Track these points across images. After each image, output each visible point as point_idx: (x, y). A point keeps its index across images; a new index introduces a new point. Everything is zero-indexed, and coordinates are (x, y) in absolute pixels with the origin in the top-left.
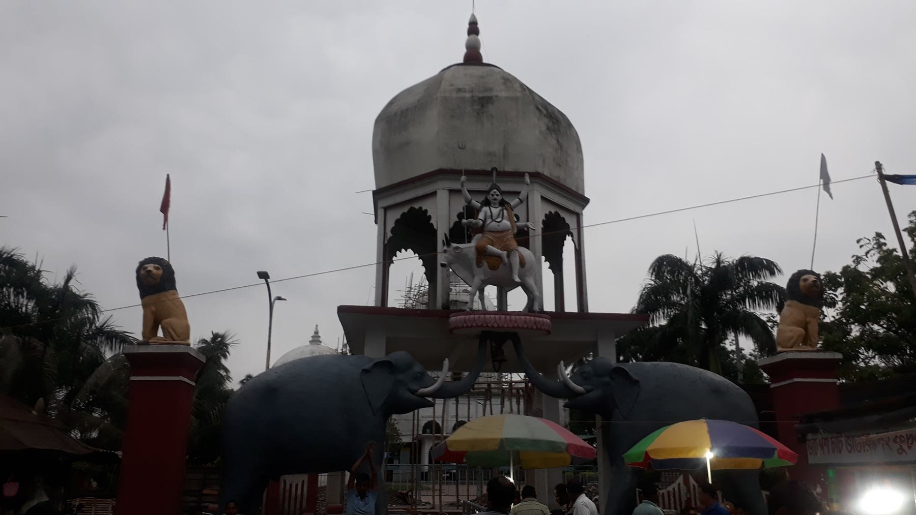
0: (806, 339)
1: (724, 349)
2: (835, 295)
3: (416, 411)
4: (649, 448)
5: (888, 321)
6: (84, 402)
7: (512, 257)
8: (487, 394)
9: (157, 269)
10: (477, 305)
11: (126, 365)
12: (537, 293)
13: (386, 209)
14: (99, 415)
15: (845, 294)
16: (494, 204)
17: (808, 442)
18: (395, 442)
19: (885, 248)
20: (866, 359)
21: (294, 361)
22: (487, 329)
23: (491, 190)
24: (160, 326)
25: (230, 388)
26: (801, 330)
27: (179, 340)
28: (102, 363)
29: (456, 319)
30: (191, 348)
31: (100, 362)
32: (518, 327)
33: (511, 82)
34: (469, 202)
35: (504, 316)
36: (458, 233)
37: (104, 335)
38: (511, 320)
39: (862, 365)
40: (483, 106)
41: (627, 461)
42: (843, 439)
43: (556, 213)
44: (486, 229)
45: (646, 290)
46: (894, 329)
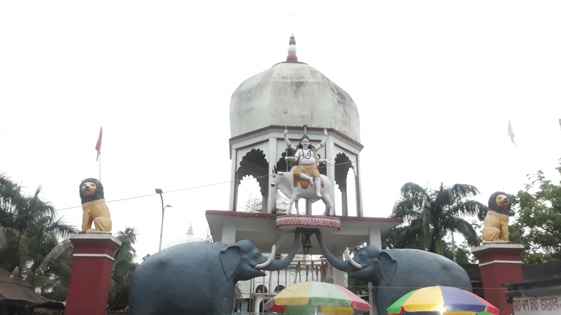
0: (501, 236)
1: (443, 242)
2: (514, 209)
3: (253, 279)
4: (404, 305)
5: (547, 225)
6: (44, 270)
7: (316, 181)
8: (298, 268)
9: (93, 185)
10: (294, 212)
11: (71, 247)
12: (331, 204)
13: (237, 150)
14: (53, 278)
15: (520, 208)
16: (305, 147)
17: (514, 303)
18: (238, 298)
19: (544, 180)
20: (534, 249)
21: (177, 245)
22: (300, 226)
23: (303, 139)
24: (93, 222)
25: (136, 262)
26: (498, 230)
27: (105, 231)
28: (56, 245)
29: (280, 219)
30: (112, 236)
31: (55, 244)
32: (320, 225)
33: (316, 73)
34: (289, 146)
35: (311, 218)
36: (282, 166)
37: (58, 227)
38: (315, 221)
39: (532, 252)
40: (298, 87)
41: (390, 312)
42: (539, 301)
44: (300, 163)
45: (397, 204)
46: (550, 230)
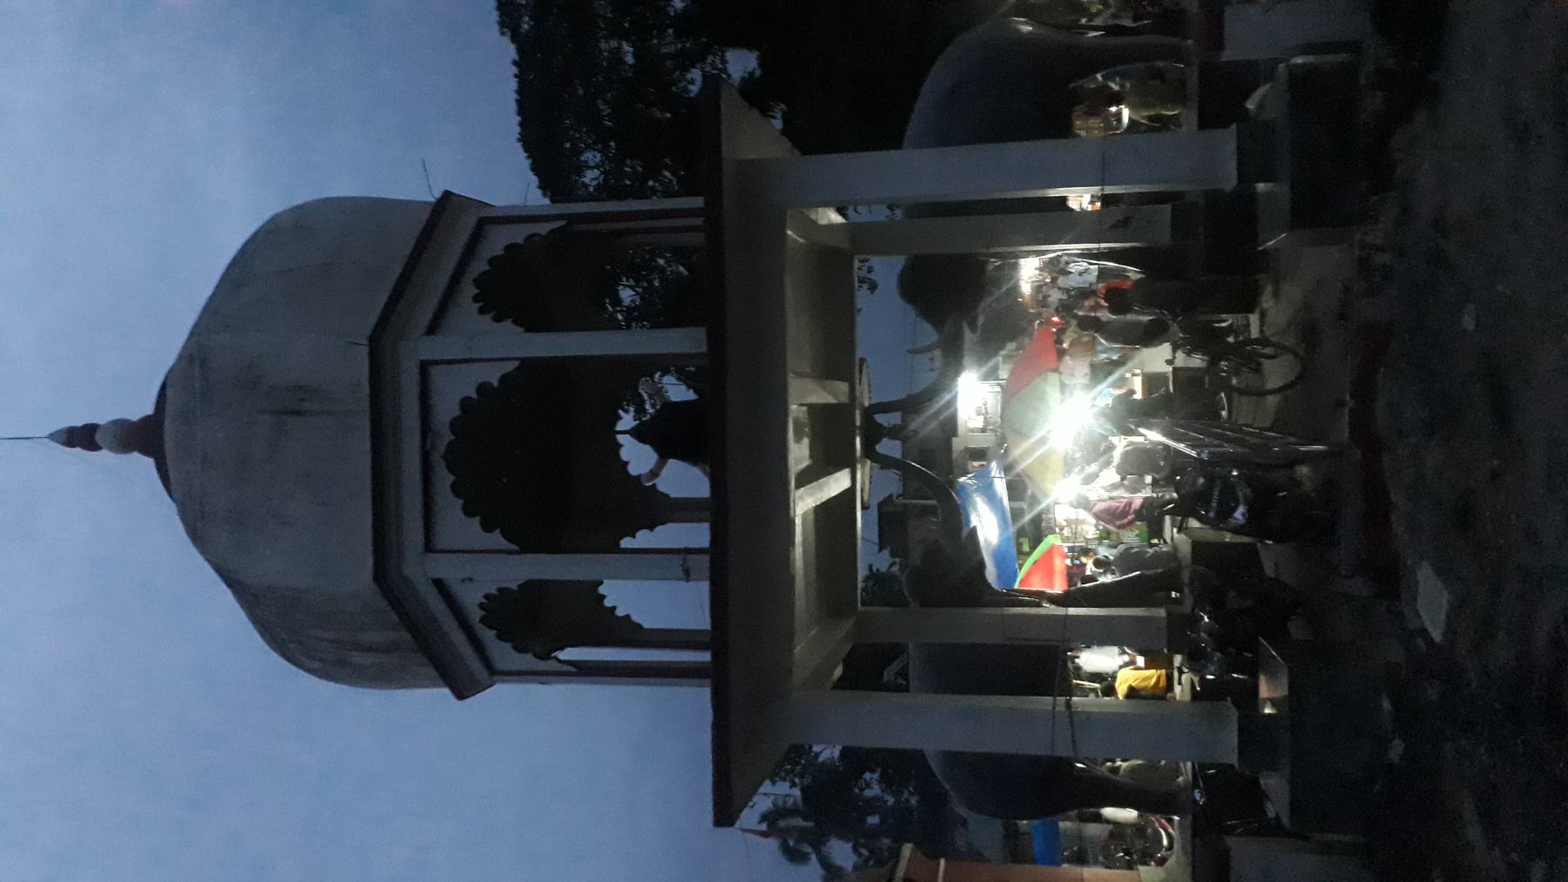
43: (477, 282)
